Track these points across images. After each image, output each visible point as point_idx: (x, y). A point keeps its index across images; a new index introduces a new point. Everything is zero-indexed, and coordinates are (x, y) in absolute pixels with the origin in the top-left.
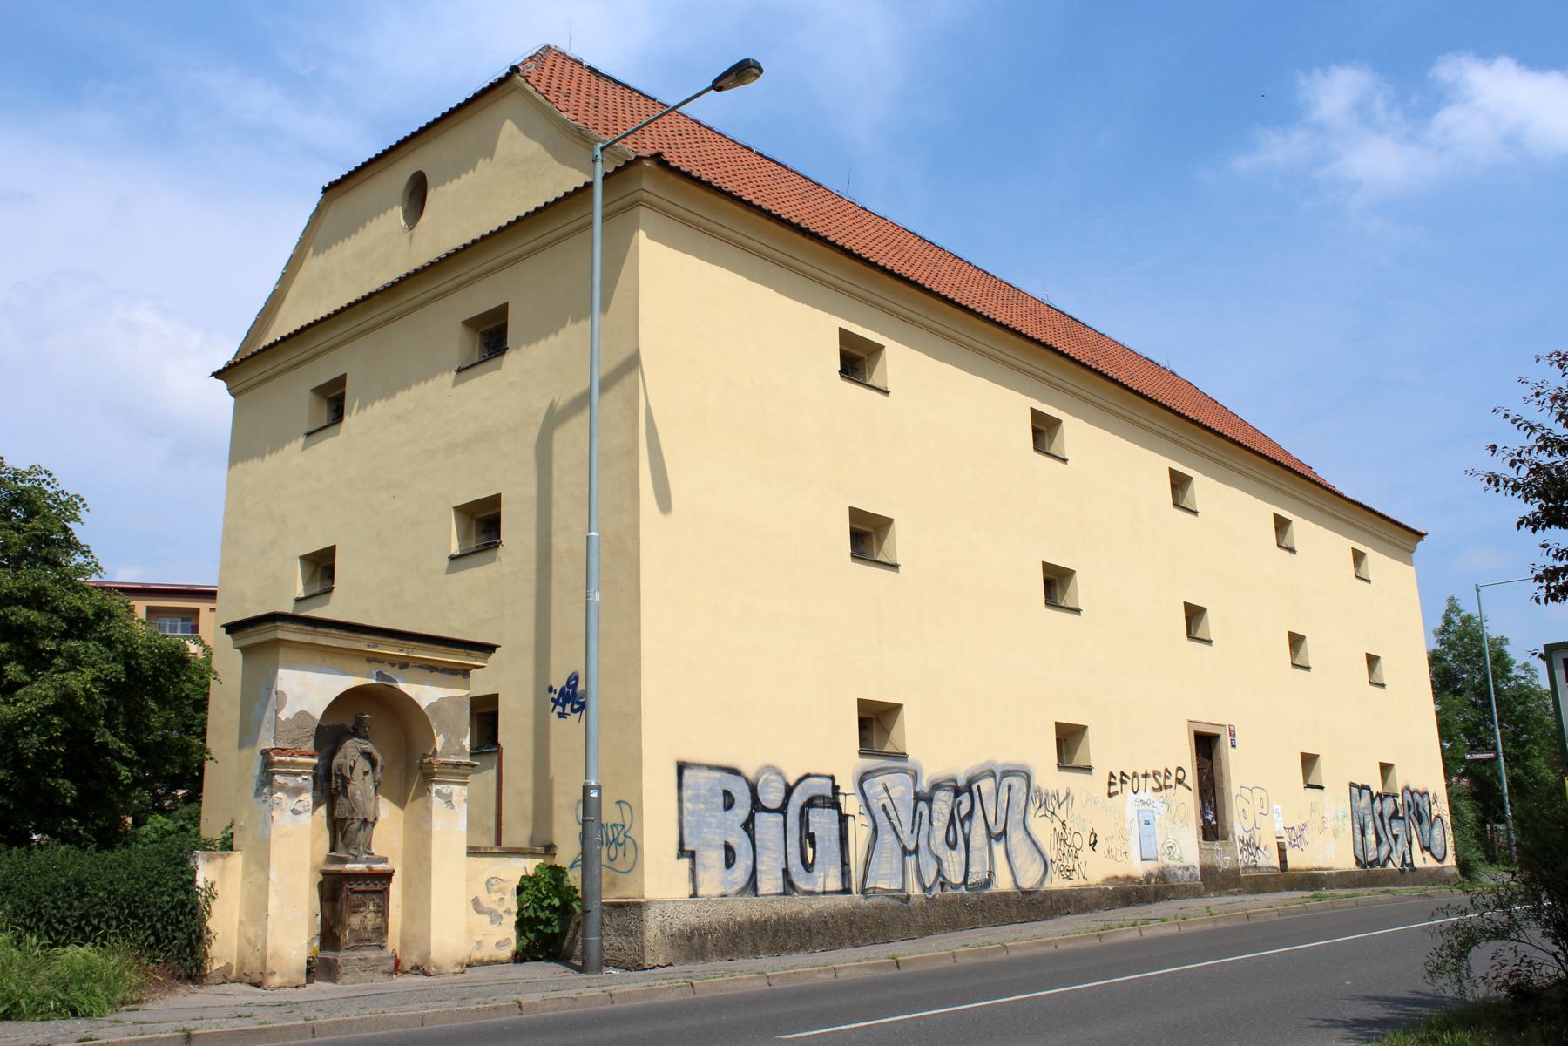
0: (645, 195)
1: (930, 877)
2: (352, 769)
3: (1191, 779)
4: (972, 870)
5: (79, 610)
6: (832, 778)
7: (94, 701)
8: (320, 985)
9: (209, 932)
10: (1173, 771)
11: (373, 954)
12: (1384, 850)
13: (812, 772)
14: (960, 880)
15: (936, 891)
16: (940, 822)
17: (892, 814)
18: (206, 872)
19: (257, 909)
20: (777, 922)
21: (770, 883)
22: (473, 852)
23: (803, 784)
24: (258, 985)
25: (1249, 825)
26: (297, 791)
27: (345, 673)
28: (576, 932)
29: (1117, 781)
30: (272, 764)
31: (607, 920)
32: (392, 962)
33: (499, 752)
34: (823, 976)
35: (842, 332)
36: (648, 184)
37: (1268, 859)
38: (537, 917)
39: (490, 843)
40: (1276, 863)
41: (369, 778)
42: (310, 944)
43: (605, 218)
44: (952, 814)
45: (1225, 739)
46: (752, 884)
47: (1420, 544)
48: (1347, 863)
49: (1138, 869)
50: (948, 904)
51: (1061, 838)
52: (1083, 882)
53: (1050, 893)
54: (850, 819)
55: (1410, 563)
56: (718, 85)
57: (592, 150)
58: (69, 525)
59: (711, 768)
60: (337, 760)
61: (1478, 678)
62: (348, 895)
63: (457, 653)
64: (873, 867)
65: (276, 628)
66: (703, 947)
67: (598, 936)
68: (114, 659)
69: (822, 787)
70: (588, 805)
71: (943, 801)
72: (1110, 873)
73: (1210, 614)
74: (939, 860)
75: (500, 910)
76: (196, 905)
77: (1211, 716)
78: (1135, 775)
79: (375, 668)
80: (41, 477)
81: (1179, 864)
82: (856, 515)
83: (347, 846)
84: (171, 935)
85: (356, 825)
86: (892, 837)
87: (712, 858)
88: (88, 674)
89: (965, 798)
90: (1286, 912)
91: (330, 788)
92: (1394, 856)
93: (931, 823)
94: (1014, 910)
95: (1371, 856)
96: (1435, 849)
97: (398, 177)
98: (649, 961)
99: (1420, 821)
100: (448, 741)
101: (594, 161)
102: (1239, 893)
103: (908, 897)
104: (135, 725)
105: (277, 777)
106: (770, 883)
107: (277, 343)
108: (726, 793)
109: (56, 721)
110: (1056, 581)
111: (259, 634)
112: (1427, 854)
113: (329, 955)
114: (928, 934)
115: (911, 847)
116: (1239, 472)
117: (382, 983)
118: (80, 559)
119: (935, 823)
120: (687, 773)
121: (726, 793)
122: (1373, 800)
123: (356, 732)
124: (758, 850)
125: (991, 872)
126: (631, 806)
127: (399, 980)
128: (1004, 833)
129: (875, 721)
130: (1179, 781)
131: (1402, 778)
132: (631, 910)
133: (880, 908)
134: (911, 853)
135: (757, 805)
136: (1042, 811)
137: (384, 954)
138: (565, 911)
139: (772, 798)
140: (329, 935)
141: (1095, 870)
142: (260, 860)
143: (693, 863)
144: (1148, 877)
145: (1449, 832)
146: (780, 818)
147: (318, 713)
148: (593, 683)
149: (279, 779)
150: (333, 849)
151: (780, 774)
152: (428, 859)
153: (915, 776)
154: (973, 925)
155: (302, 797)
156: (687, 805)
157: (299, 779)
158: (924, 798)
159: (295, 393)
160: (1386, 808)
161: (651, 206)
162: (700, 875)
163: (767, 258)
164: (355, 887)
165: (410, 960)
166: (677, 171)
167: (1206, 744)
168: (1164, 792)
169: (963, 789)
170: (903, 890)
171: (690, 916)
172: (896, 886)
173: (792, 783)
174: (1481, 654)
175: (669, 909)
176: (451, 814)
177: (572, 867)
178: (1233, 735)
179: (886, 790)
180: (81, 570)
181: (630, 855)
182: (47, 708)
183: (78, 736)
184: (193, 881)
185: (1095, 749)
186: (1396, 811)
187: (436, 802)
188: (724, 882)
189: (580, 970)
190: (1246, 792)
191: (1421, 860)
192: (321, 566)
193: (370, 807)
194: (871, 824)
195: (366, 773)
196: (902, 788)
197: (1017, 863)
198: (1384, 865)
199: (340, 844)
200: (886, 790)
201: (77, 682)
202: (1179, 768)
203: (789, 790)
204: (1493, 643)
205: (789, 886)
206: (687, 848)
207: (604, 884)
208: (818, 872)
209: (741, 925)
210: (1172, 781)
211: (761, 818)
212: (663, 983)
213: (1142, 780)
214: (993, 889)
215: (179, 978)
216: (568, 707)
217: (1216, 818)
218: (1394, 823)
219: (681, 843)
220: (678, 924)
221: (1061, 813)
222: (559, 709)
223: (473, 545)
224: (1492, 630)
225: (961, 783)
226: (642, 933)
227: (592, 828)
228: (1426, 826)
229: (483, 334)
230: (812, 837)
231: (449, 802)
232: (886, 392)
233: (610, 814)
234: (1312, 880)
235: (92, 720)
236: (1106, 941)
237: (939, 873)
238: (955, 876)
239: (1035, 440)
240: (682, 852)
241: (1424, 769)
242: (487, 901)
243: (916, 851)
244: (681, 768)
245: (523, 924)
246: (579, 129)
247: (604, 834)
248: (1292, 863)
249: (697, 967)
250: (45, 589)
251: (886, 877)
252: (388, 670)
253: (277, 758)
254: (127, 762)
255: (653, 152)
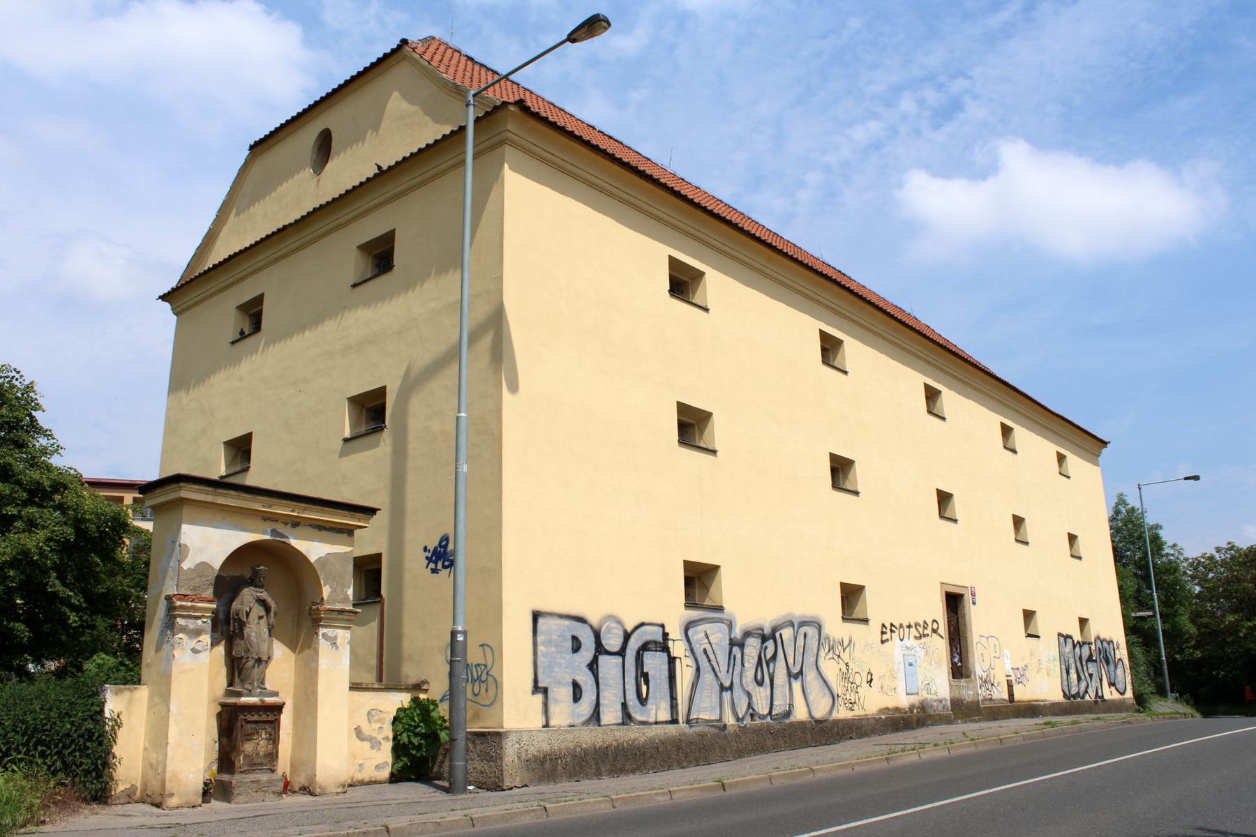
0: (510, 135)
1: (742, 709)
2: (248, 614)
3: (943, 629)
4: (775, 703)
5: (38, 483)
6: (663, 626)
7: (47, 558)
8: (215, 804)
9: (114, 757)
10: (930, 623)
11: (264, 777)
12: (1083, 685)
13: (647, 620)
14: (766, 711)
15: (747, 721)
16: (750, 664)
17: (712, 657)
18: (114, 702)
19: (158, 738)
20: (617, 748)
21: (611, 715)
22: (355, 687)
23: (638, 631)
24: (158, 805)
25: (986, 666)
26: (197, 633)
27: (242, 530)
28: (444, 756)
29: (887, 630)
30: (175, 608)
31: (471, 746)
32: (282, 784)
33: (381, 602)
34: (659, 798)
35: (671, 259)
36: (513, 126)
37: (1001, 693)
38: (410, 742)
39: (384, 673)
40: (1006, 696)
41: (263, 622)
42: (210, 767)
43: (476, 156)
44: (760, 657)
45: (968, 598)
46: (596, 716)
47: (1104, 450)
48: (1056, 696)
49: (904, 701)
50: (756, 731)
51: (845, 677)
52: (862, 713)
53: (837, 722)
54: (678, 661)
55: (1097, 464)
56: (573, 38)
57: (465, 97)
58: (34, 413)
59: (561, 616)
60: (235, 605)
61: (1138, 555)
62: (243, 726)
63: (342, 515)
64: (696, 701)
65: (180, 489)
66: (554, 770)
67: (462, 762)
68: (66, 523)
69: (655, 634)
70: (455, 647)
71: (753, 646)
72: (883, 705)
73: (956, 498)
74: (749, 695)
75: (380, 738)
76: (102, 734)
77: (958, 580)
78: (901, 626)
79: (269, 526)
80: (11, 374)
81: (935, 697)
82: (683, 408)
83: (242, 681)
84: (80, 762)
85: (251, 663)
86: (712, 676)
87: (563, 693)
88: (41, 535)
89: (770, 644)
90: (1030, 737)
91: (227, 629)
92: (1090, 690)
93: (743, 664)
94: (809, 736)
95: (1074, 691)
96: (1118, 685)
97: (308, 136)
98: (507, 783)
99: (1108, 663)
100: (333, 591)
101: (468, 105)
102: (979, 721)
103: (725, 726)
104: (85, 578)
105: (178, 620)
106: (611, 715)
107: (210, 269)
108: (575, 638)
109: (12, 573)
110: (840, 468)
111: (168, 493)
112: (1113, 689)
113: (225, 777)
114: (740, 757)
115: (727, 684)
116: (975, 389)
117: (272, 803)
118: (43, 441)
119: (746, 664)
120: (541, 621)
121: (575, 638)
122: (1074, 646)
123: (253, 582)
124: (601, 687)
125: (791, 705)
126: (493, 649)
127: (288, 799)
128: (801, 672)
129: (698, 578)
130: (934, 631)
131: (1095, 630)
132: (491, 740)
133: (702, 735)
134: (727, 689)
135: (600, 649)
136: (830, 655)
137: (274, 776)
138: (432, 737)
139: (613, 642)
140: (226, 761)
141: (872, 702)
142: (163, 695)
143: (546, 698)
144: (912, 707)
145: (1128, 671)
146: (620, 659)
147: (217, 564)
148: (461, 543)
149: (180, 621)
150: (231, 684)
151: (619, 622)
152: (315, 693)
153: (730, 626)
154: (776, 748)
155: (200, 638)
156: (541, 648)
157: (199, 622)
158: (737, 643)
159: (223, 314)
160: (1084, 653)
161: (515, 145)
162: (553, 708)
163: (610, 195)
164: (249, 717)
165: (300, 780)
166: (536, 116)
167: (954, 602)
168: (923, 640)
169: (768, 636)
170: (720, 720)
171: (543, 744)
172: (715, 717)
173: (629, 630)
174: (1140, 537)
175: (525, 738)
176: (336, 654)
177: (441, 701)
178: (973, 594)
179: (707, 637)
180: (44, 451)
181: (492, 692)
182: (6, 562)
183: (33, 587)
184: (102, 712)
185: (872, 604)
186: (1091, 655)
187: (323, 645)
188: (572, 714)
189: (447, 790)
190: (984, 640)
191: (1109, 694)
192: (240, 448)
193: (265, 646)
194: (694, 665)
195: (261, 618)
196: (720, 635)
197: (811, 698)
198: (1083, 697)
199: (237, 680)
200: (707, 637)
201: (33, 541)
202: (934, 621)
203: (627, 636)
204: (1151, 528)
205: (627, 717)
206: (541, 685)
207: (469, 716)
208: (651, 705)
209: (586, 751)
210: (928, 631)
211: (603, 659)
212: (518, 804)
213: (907, 630)
214: (792, 719)
215: (85, 800)
216: (440, 564)
217: (961, 660)
218: (1090, 665)
219: (536, 681)
220: (532, 750)
221: (845, 656)
222: (432, 565)
223: (363, 429)
224: (1150, 520)
225: (767, 631)
226: (501, 759)
227: (460, 669)
228: (1112, 667)
229: (375, 257)
230: (646, 676)
231: (334, 644)
232: (706, 310)
233: (474, 656)
234: (1032, 710)
235: (45, 572)
236: (893, 763)
237: (750, 706)
238: (762, 708)
239: (823, 356)
240: (536, 688)
241: (1110, 625)
242: (367, 729)
243: (731, 688)
244: (536, 616)
245: (399, 749)
246: (456, 86)
247: (471, 671)
248: (1018, 696)
249: (548, 788)
250: (10, 465)
251: (706, 710)
252: (281, 528)
253: (178, 603)
254: (74, 608)
255: (517, 98)
